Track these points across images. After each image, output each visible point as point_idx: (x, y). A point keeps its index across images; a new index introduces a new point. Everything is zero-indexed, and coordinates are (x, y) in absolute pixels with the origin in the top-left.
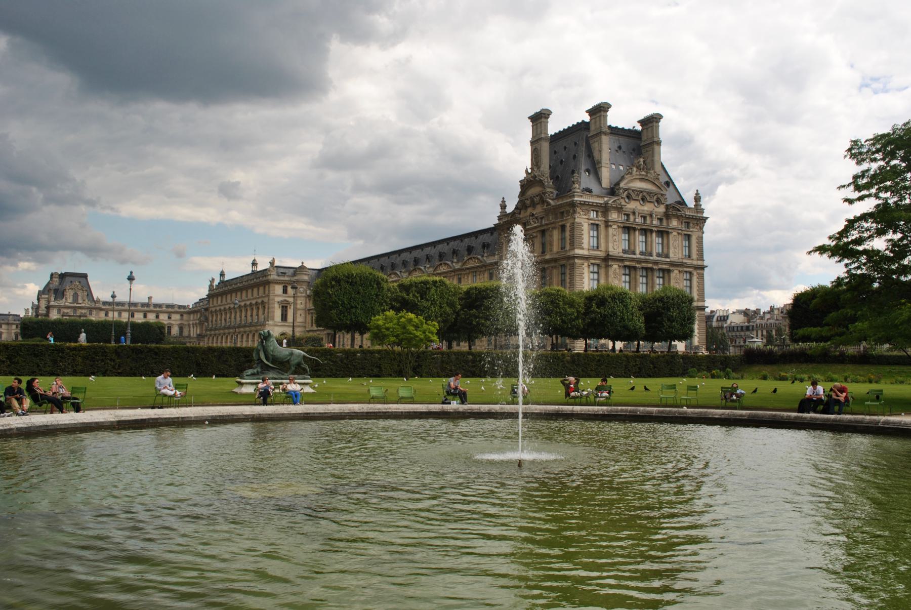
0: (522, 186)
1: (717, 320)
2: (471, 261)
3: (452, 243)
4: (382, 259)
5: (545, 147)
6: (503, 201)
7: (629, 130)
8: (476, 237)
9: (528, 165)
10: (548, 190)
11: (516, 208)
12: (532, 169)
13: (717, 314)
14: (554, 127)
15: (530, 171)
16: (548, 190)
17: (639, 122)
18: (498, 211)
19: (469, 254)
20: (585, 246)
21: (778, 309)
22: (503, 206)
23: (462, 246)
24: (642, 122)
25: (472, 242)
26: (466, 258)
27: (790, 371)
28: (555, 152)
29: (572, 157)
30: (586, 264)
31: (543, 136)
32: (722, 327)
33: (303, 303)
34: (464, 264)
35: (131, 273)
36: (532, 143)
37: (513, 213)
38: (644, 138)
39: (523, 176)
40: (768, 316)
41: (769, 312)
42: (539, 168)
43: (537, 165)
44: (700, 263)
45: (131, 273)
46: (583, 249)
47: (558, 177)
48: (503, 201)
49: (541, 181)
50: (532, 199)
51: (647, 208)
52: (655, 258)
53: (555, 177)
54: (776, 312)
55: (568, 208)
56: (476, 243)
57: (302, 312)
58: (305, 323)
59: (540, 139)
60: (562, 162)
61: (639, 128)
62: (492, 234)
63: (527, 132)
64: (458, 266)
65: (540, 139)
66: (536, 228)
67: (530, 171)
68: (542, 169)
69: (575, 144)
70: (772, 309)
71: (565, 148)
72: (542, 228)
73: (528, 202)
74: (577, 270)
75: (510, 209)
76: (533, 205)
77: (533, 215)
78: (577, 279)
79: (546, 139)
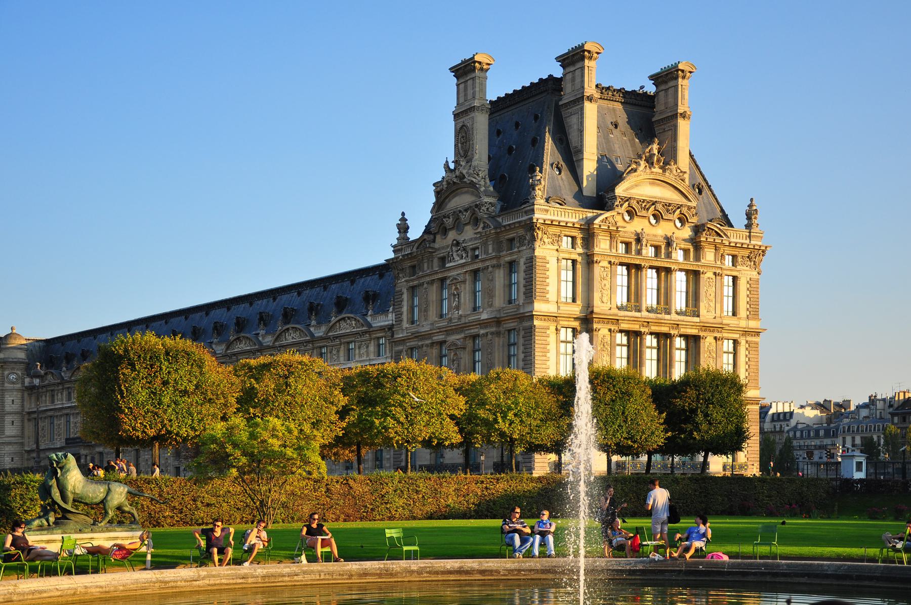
0: (438, 193)
1: (773, 420)
2: (343, 324)
3: (307, 292)
4: (284, 298)
5: (481, 124)
6: (403, 219)
7: (634, 92)
8: (353, 282)
9: (450, 155)
10: (487, 199)
11: (427, 231)
12: (455, 162)
13: (772, 411)
14: (496, 88)
15: (452, 166)
16: (487, 199)
17: (652, 78)
18: (393, 237)
19: (340, 312)
20: (552, 296)
21: (884, 400)
22: (403, 228)
23: (327, 297)
24: (657, 79)
25: (346, 290)
26: (334, 320)
27: (834, 555)
28: (499, 133)
29: (529, 140)
30: (553, 328)
31: (476, 103)
32: (781, 431)
33: (18, 401)
34: (330, 329)
35: (403, 214)
36: (457, 116)
37: (421, 241)
38: (659, 107)
39: (440, 174)
40: (864, 413)
41: (865, 406)
42: (469, 161)
43: (465, 156)
44: (753, 324)
45: (403, 214)
46: (547, 301)
47: (503, 177)
48: (403, 219)
49: (473, 185)
50: (456, 214)
51: (664, 229)
52: (674, 316)
53: (495, 175)
54: (880, 405)
55: (521, 232)
56: (355, 291)
57: (16, 419)
58: (22, 436)
59: (472, 109)
60: (510, 150)
61: (651, 89)
62: (381, 276)
63: (447, 94)
64: (319, 332)
65: (472, 109)
66: (463, 265)
67: (452, 166)
68: (474, 163)
69: (536, 118)
70: (873, 401)
71: (517, 125)
72: (475, 267)
73: (449, 222)
74: (538, 339)
75: (415, 233)
76: (458, 226)
77: (458, 244)
78: (538, 353)
79: (481, 108)
